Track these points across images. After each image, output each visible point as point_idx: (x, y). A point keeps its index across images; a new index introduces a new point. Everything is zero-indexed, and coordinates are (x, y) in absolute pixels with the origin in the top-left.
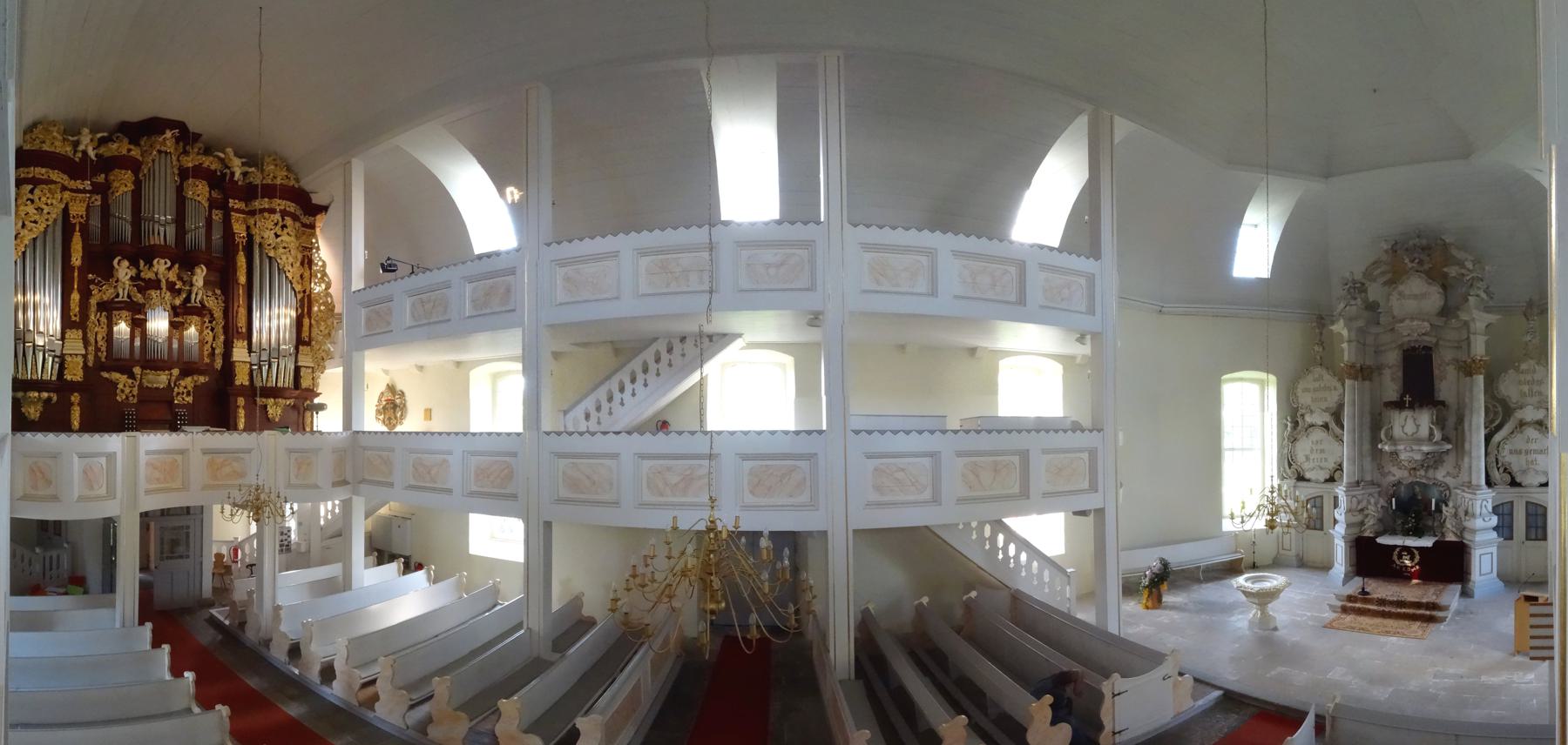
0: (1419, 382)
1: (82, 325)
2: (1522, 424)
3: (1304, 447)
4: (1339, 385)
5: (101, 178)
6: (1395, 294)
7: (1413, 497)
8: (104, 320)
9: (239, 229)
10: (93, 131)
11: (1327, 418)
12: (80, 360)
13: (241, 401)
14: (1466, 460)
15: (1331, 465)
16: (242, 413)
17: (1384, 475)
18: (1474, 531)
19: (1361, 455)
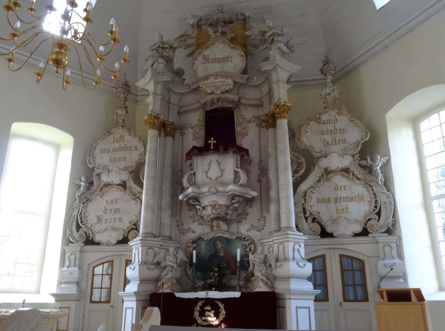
0: (220, 130)
2: (327, 172)
3: (96, 208)
4: (140, 146)
6: (200, 58)
7: (215, 255)
11: (125, 176)
14: (273, 207)
15: (126, 225)
17: (183, 232)
18: (287, 278)
19: (160, 208)
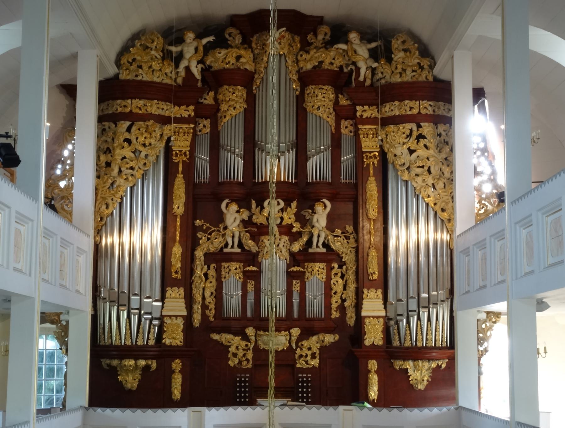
1: (187, 282)
5: (208, 99)
8: (212, 273)
9: (370, 145)
10: (199, 36)
12: (180, 322)
13: (373, 365)
16: (374, 379)
